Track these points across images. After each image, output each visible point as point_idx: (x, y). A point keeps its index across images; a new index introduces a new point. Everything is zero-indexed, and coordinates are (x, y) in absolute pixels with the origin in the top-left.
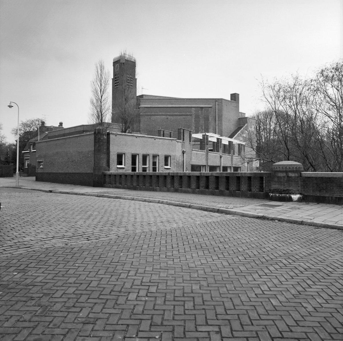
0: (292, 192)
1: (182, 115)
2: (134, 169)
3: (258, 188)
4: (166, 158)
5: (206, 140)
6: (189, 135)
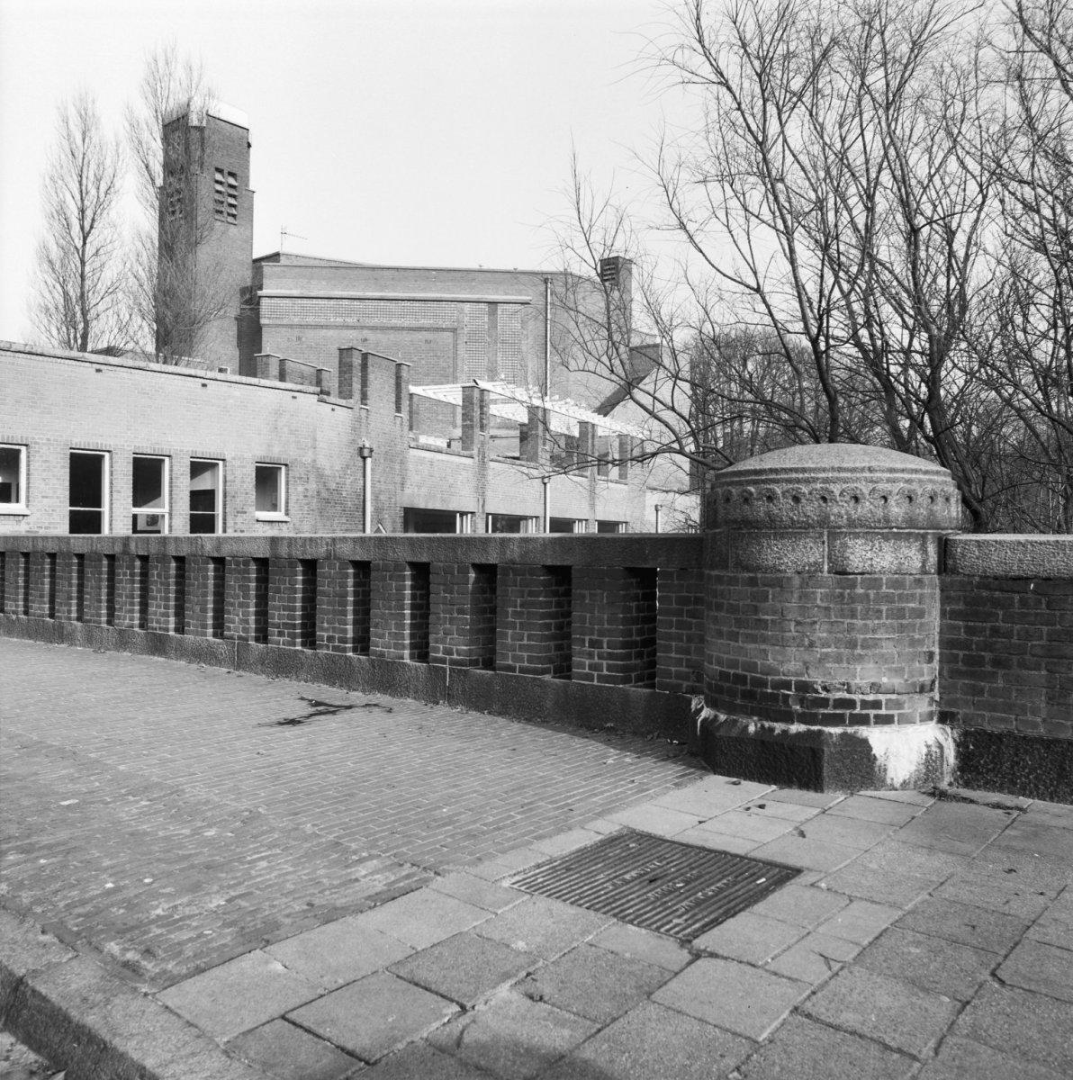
0: (877, 705)
1: (419, 329)
2: (85, 522)
3: (611, 656)
4: (266, 477)
5: (477, 409)
6: (393, 381)
